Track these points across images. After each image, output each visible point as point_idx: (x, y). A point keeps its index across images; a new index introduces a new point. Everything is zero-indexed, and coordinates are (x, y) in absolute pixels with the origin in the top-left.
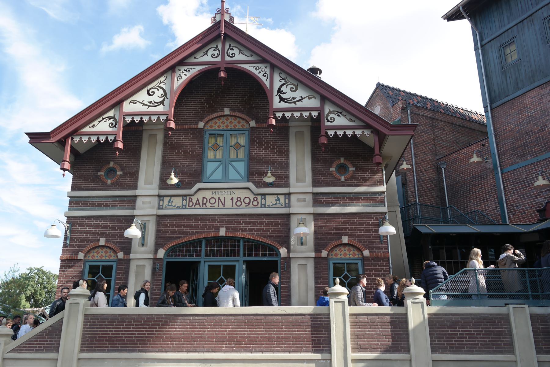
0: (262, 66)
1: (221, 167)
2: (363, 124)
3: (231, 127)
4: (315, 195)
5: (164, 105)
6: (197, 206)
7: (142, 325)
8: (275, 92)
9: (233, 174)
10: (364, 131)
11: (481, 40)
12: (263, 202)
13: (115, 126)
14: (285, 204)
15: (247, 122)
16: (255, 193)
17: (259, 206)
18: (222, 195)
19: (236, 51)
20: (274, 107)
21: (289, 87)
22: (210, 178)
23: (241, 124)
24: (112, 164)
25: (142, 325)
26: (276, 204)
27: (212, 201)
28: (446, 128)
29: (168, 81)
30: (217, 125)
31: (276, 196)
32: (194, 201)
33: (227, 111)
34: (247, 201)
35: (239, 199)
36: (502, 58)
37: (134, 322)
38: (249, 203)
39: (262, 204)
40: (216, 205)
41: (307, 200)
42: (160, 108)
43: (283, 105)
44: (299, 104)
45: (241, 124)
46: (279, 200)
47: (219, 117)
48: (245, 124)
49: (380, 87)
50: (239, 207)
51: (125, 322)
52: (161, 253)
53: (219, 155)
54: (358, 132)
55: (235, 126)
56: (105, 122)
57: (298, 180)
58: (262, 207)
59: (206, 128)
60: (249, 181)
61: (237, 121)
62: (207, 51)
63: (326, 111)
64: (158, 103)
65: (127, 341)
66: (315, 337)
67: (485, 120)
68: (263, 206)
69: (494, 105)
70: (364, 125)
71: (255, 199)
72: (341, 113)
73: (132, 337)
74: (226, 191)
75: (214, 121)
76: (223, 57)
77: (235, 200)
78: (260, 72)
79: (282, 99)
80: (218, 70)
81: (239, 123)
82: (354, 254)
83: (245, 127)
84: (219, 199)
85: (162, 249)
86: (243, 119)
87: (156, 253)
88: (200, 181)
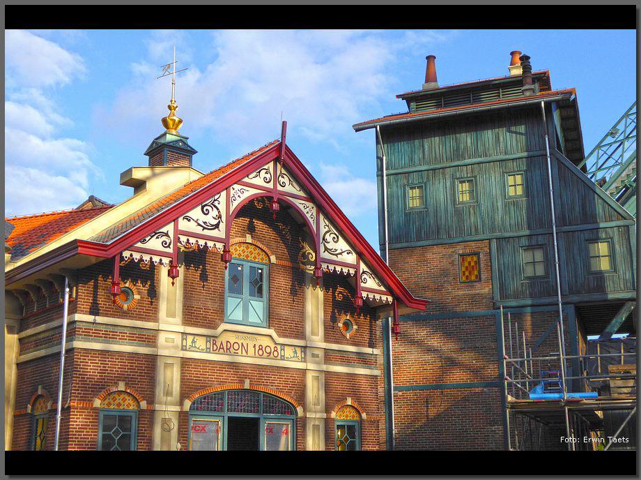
0: (310, 205)
5: (219, 230)
6: (221, 351)
8: (321, 241)
9: (253, 318)
10: (388, 297)
17: (279, 357)
19: (286, 180)
21: (333, 236)
26: (294, 357)
31: (293, 348)
38: (270, 353)
40: (239, 351)
42: (214, 233)
44: (340, 258)
46: (296, 353)
56: (157, 238)
58: (281, 359)
62: (259, 172)
64: (213, 226)
71: (276, 349)
74: (249, 335)
76: (275, 185)
77: (257, 348)
78: (308, 213)
84: (242, 345)
87: (181, 404)
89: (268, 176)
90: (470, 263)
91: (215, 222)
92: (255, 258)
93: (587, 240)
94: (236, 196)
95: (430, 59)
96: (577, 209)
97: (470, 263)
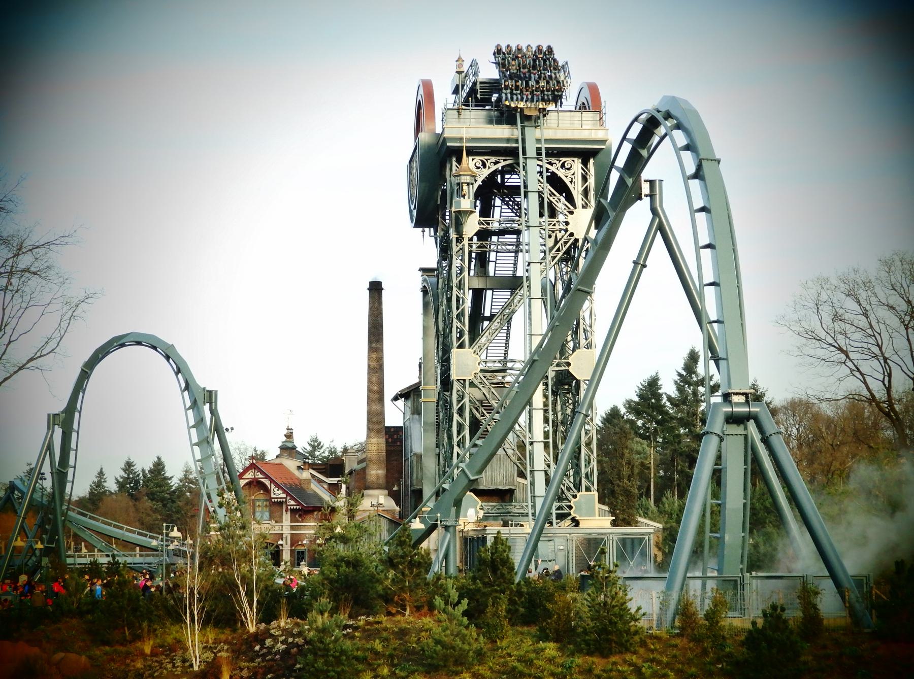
2: (558, 240)
4: (291, 526)
19: (259, 473)
44: (280, 496)
57: (286, 520)
85: (465, 484)
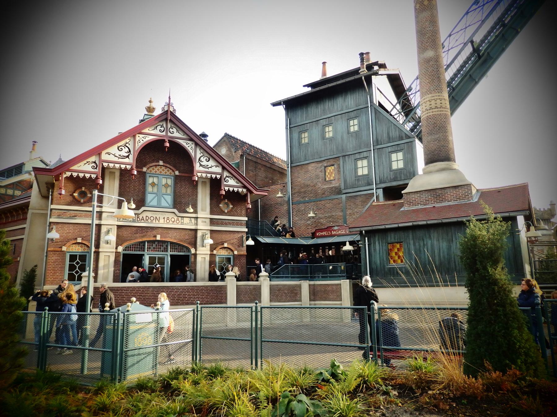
1: (157, 197)
3: (163, 173)
5: (129, 158)
6: (143, 221)
7: (129, 292)
8: (197, 160)
10: (243, 189)
11: (290, 125)
12: (182, 221)
13: (96, 168)
14: (195, 223)
15: (173, 171)
16: (173, 214)
18: (158, 215)
19: (175, 130)
20: (197, 169)
21: (205, 158)
22: (150, 204)
23: (169, 172)
24: (83, 189)
25: (129, 292)
26: (190, 223)
27: (152, 218)
28: (262, 169)
29: (131, 143)
30: (154, 170)
32: (141, 218)
33: (161, 163)
34: (173, 220)
35: (168, 218)
36: (300, 139)
37: (124, 291)
38: (174, 221)
39: (181, 223)
40: (154, 221)
41: (207, 222)
42: (127, 160)
43: (202, 169)
44: (210, 170)
45: (169, 172)
46: (191, 221)
47: (156, 166)
48: (172, 172)
49: (227, 136)
50: (168, 223)
51: (119, 291)
52: (120, 249)
53: (155, 190)
54: (240, 190)
55: (166, 173)
57: (202, 210)
58: (181, 224)
59: (147, 172)
60: (174, 208)
61: (167, 169)
62: (156, 127)
63: (225, 176)
65: (121, 301)
66: (171, 300)
67: (285, 166)
68: (182, 224)
69: (293, 165)
70: (242, 186)
71: (168, 219)
72: (232, 177)
73: (124, 299)
75: (152, 168)
76: (167, 133)
77: (166, 219)
78: (189, 146)
79: (201, 165)
80: (163, 141)
81: (168, 171)
82: (229, 253)
83: (172, 174)
84: (156, 217)
86: (171, 169)
87: (116, 248)
88: (144, 205)
89: (162, 129)
90: (330, 170)
91: (127, 154)
92: (156, 172)
93: (390, 152)
94: (141, 141)
95: (324, 63)
96: (385, 135)
97: (330, 170)
